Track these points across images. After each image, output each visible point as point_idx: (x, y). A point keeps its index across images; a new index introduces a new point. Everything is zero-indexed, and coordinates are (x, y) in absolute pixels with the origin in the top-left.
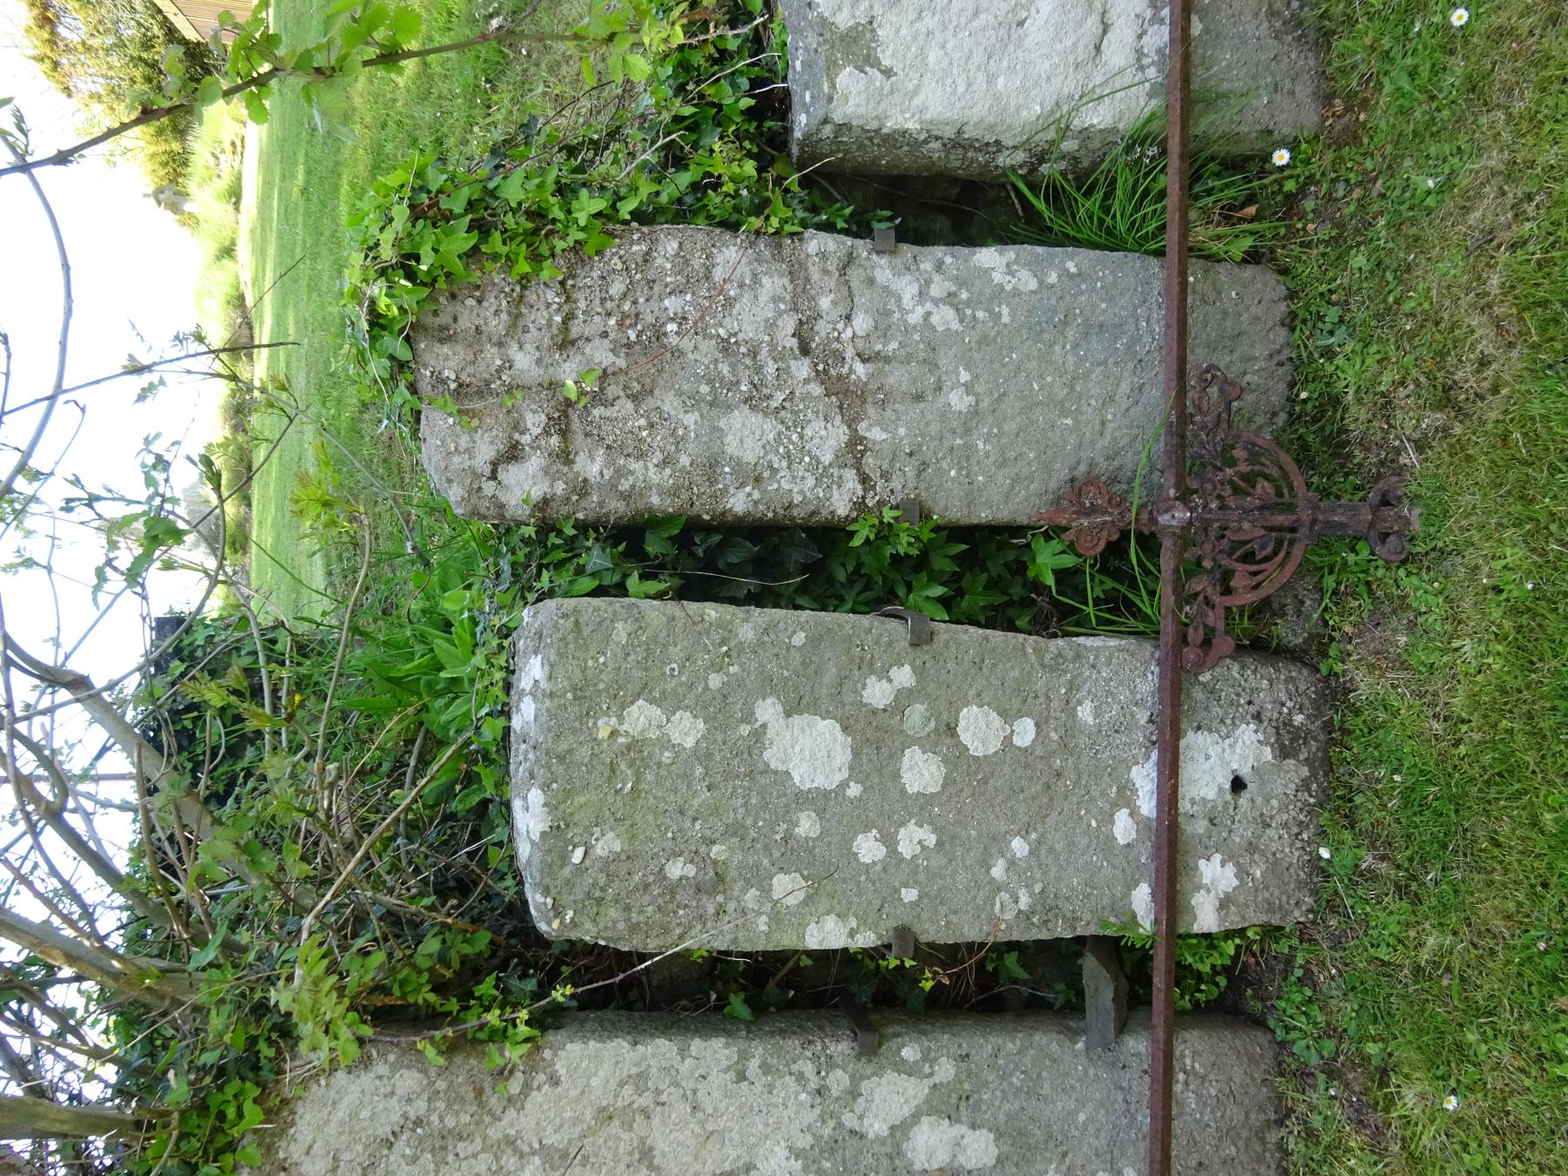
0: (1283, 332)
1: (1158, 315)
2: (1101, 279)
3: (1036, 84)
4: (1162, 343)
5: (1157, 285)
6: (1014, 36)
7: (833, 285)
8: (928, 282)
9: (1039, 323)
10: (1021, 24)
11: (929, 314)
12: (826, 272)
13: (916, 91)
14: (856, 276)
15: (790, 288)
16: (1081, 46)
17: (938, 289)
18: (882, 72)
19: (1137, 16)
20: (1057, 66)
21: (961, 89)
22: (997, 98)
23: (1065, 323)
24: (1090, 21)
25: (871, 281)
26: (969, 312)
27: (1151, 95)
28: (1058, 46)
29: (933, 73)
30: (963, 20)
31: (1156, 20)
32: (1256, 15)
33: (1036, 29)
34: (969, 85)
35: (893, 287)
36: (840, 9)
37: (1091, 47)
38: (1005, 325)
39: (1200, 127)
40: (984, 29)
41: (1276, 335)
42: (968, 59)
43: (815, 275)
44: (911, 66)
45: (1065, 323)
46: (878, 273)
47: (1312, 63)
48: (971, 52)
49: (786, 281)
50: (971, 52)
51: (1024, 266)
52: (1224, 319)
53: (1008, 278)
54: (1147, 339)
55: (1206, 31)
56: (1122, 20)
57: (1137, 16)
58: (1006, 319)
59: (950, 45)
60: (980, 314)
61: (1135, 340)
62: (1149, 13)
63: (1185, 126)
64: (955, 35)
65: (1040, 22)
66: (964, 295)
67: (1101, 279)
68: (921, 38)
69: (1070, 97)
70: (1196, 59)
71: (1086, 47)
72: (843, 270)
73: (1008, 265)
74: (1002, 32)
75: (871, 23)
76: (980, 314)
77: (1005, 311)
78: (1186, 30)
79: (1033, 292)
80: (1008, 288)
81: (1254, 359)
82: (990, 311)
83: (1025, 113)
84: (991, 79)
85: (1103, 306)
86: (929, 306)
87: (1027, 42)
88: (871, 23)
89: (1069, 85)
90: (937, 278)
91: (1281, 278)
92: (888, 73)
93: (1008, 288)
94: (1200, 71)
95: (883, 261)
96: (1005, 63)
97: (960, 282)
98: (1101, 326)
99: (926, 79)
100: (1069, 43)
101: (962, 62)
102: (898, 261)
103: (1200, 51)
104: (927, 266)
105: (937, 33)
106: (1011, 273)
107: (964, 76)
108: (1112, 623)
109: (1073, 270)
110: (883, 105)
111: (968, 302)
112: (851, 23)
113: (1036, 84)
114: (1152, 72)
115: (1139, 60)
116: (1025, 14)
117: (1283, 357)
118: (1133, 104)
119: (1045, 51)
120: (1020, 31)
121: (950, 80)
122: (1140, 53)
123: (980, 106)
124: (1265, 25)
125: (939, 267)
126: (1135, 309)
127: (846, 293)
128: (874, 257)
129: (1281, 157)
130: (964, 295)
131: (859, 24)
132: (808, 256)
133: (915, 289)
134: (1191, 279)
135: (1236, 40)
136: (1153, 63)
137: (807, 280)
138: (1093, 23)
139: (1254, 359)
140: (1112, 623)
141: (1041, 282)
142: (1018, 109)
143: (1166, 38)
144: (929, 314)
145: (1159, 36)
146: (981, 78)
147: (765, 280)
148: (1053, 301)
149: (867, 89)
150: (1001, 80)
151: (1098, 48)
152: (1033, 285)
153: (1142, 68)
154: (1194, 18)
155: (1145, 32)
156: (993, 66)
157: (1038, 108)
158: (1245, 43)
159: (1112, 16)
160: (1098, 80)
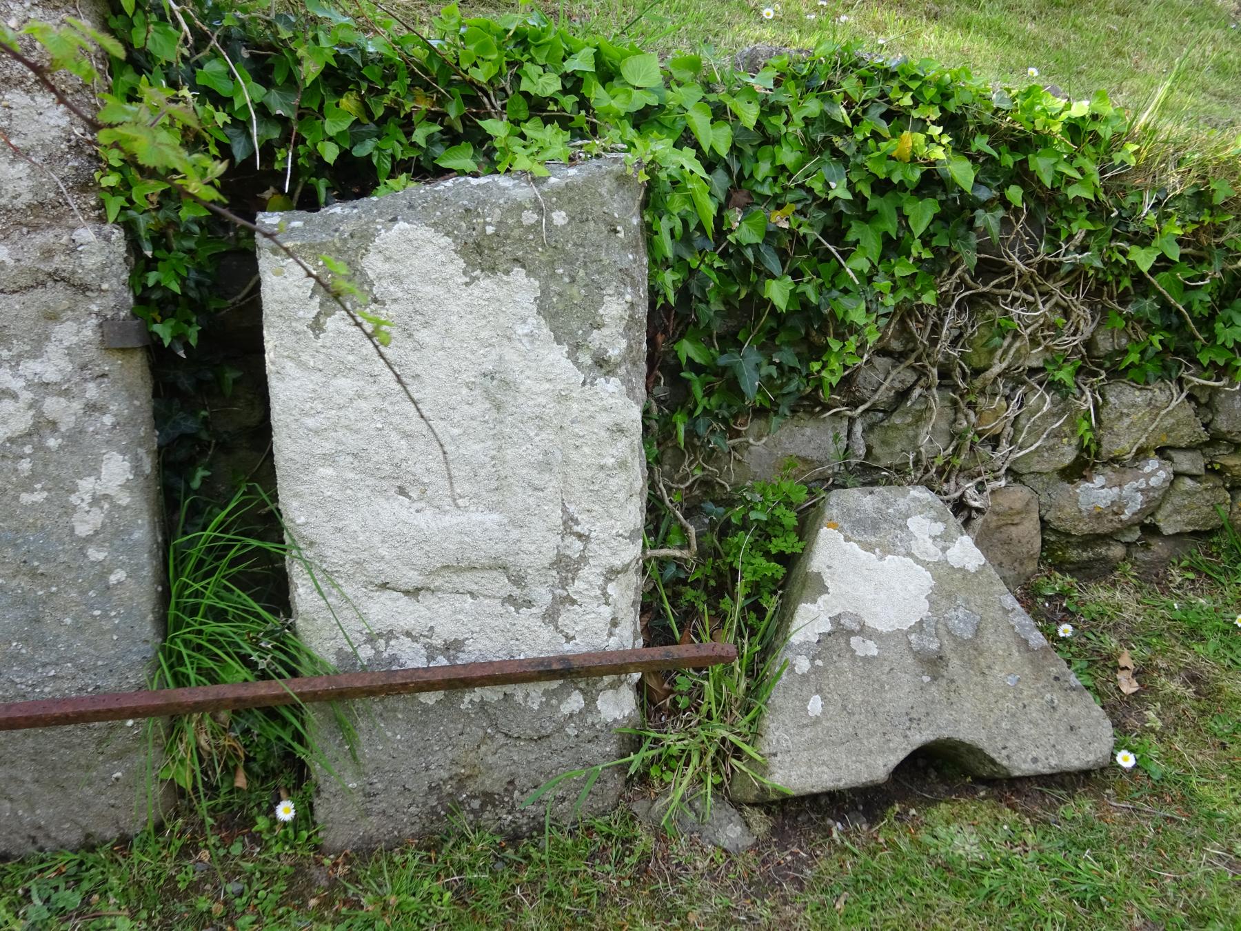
0: (75, 837)
1: (68, 688)
2: (105, 615)
3: (331, 516)
4: (30, 698)
5: (111, 683)
6: (385, 484)
7: (27, 263)
8: (66, 393)
9: (26, 541)
10: (402, 491)
11: (14, 396)
12: (48, 253)
13: (302, 365)
14: (57, 296)
15: (19, 203)
16: (383, 566)
17: (53, 406)
18: (317, 318)
19: (432, 628)
20: (355, 539)
21: (310, 422)
22: (306, 468)
23: (34, 574)
24: (413, 574)
25: (53, 317)
26: (28, 450)
27: (339, 652)
28: (377, 539)
29: (325, 385)
30: (396, 420)
31: (431, 652)
32: (454, 762)
33: (395, 510)
34: (317, 432)
35: (51, 348)
36: (388, 259)
37: (382, 578)
38: (16, 498)
39: (312, 714)
40: (388, 446)
41: (69, 831)
42: (347, 427)
43: (39, 239)
44: (329, 356)
45: (34, 574)
46: (70, 327)
47: (408, 831)
48: (357, 432)
49: (27, 197)
50: (357, 432)
51: (109, 515)
52: (80, 767)
53: (88, 498)
54: (31, 678)
55: (426, 710)
56: (424, 612)
57: (432, 628)
58: (26, 498)
59: (363, 404)
60: (25, 465)
61: (27, 664)
62: (437, 642)
63: (314, 697)
64: (375, 410)
65: (404, 514)
66: (52, 443)
67: (105, 615)
68: (365, 367)
69: (323, 558)
70: (391, 701)
71: (381, 572)
72: (56, 277)
73: (106, 497)
74: (387, 469)
75: (375, 301)
76: (25, 465)
77: (39, 497)
78: (430, 686)
79: (72, 529)
80: (73, 499)
81: (32, 809)
82: (34, 476)
83: (295, 504)
84: (329, 459)
85: (68, 621)
86: (27, 396)
87: (381, 500)
88: (375, 301)
89: (334, 557)
90: (77, 406)
91: (150, 827)
92: (317, 326)
93: (73, 499)
94: (378, 708)
95: (89, 331)
96: (351, 475)
97: (75, 438)
98: (37, 621)
99: (317, 377)
100: (383, 551)
101: (343, 422)
102: (93, 353)
103: (401, 705)
104: (92, 391)
105: (375, 387)
106: (96, 501)
107: (326, 424)
108: (244, 611)
109: (113, 579)
110: (279, 322)
111: (40, 448)
112: (372, 275)
113: (331, 516)
114: (366, 653)
115: (380, 635)
116: (414, 496)
117: (42, 842)
118: (325, 634)
119: (370, 522)
120: (392, 492)
121: (319, 407)
122: (390, 635)
123: (293, 447)
124: (445, 775)
125: (93, 408)
126: (71, 660)
127: (22, 282)
128: (94, 321)
129: (286, 811)
130: (52, 443)
131: (372, 285)
132: (72, 229)
133: (51, 375)
134: (130, 723)
135: (421, 744)
136: (378, 653)
137: (36, 228)
138: (413, 578)
139: (32, 809)
140: (244, 611)
141: (88, 540)
142: (296, 495)
143: (411, 665)
144: (14, 396)
145: (412, 657)
146: (329, 446)
147: (22, 168)
148: (63, 558)
149: (293, 300)
150: (329, 472)
151: (384, 586)
152: (83, 530)
153: (371, 639)
154: (440, 695)
155: (415, 639)
156: (345, 460)
157: (302, 520)
158: (419, 754)
159: (427, 599)
160: (349, 590)
